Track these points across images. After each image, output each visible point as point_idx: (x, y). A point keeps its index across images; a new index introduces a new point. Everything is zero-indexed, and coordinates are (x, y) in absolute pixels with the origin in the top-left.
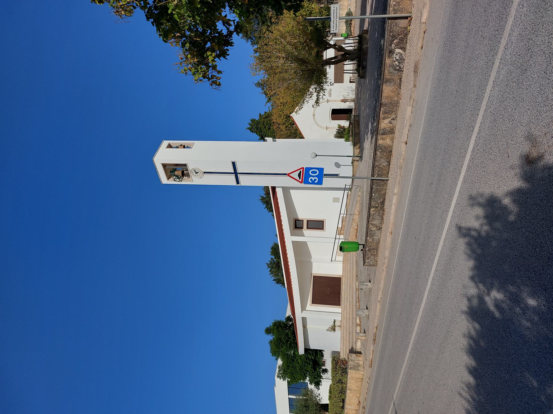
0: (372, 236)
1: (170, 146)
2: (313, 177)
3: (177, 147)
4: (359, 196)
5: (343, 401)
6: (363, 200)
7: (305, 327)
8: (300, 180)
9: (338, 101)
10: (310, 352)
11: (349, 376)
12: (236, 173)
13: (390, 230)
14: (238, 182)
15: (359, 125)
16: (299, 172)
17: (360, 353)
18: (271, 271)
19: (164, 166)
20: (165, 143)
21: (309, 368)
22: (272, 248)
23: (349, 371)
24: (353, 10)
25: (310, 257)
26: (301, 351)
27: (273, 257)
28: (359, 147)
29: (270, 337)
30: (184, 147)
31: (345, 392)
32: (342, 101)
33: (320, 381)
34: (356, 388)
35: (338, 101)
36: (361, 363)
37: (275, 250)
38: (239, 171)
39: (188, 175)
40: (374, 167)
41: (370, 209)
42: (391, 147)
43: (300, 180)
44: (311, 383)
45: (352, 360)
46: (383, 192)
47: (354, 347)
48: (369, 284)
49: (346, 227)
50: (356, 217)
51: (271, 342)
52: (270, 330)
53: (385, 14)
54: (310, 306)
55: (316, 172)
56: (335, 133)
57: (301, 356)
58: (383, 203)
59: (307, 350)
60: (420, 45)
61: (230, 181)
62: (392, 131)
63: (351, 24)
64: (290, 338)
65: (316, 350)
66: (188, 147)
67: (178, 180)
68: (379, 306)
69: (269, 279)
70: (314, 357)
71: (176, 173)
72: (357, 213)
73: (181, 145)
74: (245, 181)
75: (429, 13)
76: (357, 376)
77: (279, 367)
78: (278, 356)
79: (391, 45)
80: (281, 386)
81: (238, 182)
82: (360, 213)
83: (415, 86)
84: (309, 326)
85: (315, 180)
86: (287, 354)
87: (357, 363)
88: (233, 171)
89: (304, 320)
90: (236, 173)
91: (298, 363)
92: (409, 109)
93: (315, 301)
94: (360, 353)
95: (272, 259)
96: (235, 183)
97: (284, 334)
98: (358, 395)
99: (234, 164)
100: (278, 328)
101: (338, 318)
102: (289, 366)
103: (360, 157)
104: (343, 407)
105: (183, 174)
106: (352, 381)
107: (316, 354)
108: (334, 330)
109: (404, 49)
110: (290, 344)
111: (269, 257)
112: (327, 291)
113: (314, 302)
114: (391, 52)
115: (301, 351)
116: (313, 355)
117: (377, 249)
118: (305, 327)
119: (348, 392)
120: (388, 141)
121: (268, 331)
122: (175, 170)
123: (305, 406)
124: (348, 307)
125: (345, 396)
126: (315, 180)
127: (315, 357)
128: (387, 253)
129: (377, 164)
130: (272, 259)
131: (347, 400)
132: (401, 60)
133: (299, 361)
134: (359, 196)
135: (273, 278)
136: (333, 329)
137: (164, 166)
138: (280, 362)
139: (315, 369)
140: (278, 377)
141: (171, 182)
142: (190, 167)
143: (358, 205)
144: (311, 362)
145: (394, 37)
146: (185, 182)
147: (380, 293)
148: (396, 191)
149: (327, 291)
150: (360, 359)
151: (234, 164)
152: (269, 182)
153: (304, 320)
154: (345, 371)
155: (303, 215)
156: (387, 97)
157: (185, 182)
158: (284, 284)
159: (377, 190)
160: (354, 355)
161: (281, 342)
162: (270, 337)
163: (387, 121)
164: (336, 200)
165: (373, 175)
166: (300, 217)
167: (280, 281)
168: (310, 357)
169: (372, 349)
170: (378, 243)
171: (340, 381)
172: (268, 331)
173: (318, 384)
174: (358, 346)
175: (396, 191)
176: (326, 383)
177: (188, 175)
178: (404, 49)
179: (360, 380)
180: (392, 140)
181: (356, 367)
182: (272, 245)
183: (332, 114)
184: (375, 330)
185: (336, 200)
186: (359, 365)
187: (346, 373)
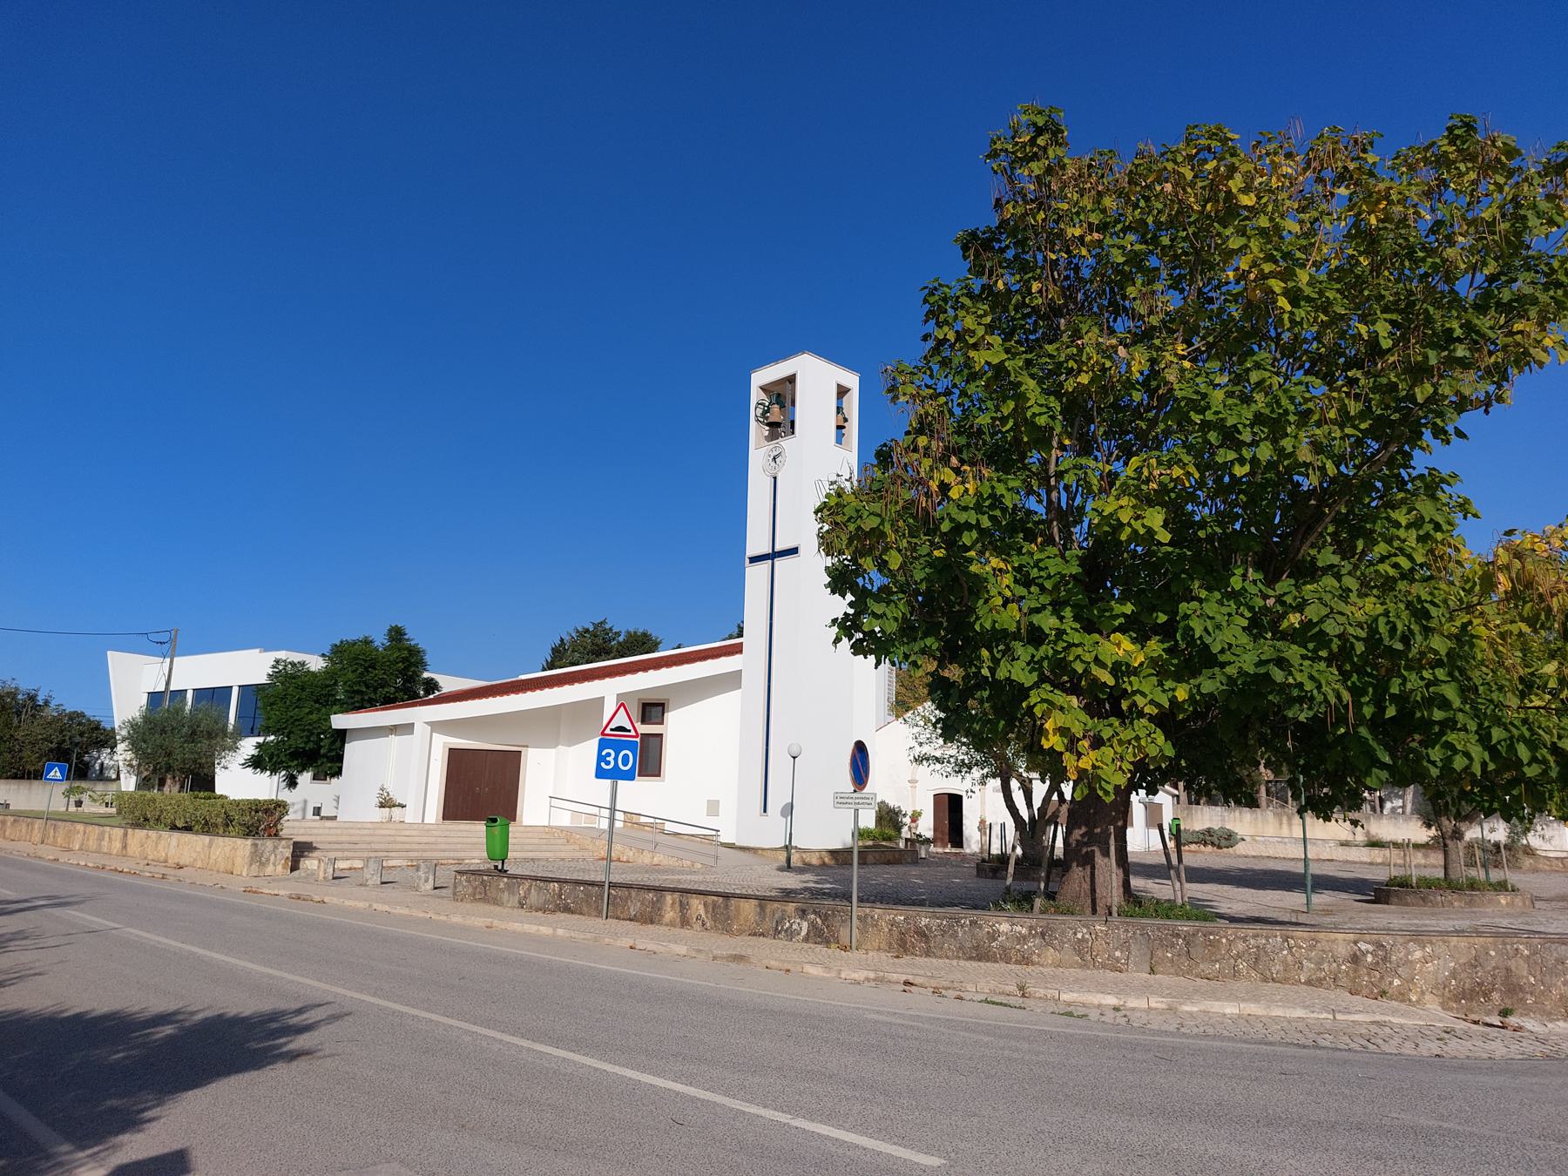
0: (509, 887)
1: (842, 392)
2: (616, 759)
3: (839, 409)
4: (693, 863)
5: (188, 829)
6: (679, 873)
7: (394, 729)
8: (608, 731)
9: (983, 810)
10: (338, 744)
11: (239, 841)
12: (773, 556)
13: (496, 923)
14: (754, 560)
15: (889, 863)
16: (629, 727)
17: (294, 868)
18: (587, 631)
19: (791, 379)
20: (852, 380)
21: (297, 742)
22: (645, 634)
23: (249, 842)
24: (1240, 848)
25: (571, 742)
26: (339, 721)
27: (621, 639)
28: (824, 864)
29: (380, 640)
30: (840, 427)
31: (208, 833)
32: (982, 822)
33: (263, 769)
34: (213, 857)
35: (983, 810)
36: (269, 870)
37: (642, 642)
38: (779, 562)
39: (773, 436)
40: (629, 887)
41: (558, 881)
42: (660, 923)
43: (608, 731)
44: (259, 746)
45: (276, 848)
46: (585, 909)
47: (316, 854)
48: (430, 885)
49: (639, 834)
50: (646, 859)
51: (367, 642)
52: (400, 640)
53: (861, 900)
54: (442, 743)
55: (625, 764)
56: (891, 805)
57: (328, 720)
58: (567, 909)
59: (342, 736)
60: (772, 963)
61: (757, 543)
62: (685, 922)
63: (1205, 844)
64: (375, 691)
65: (340, 758)
66: (839, 441)
67: (760, 411)
68: (361, 905)
69: (566, 628)
70: (320, 755)
71: (776, 408)
72: (656, 861)
73: (846, 420)
74: (756, 576)
75: (816, 978)
76: (238, 861)
77: (303, 664)
78: (331, 659)
79: (815, 912)
80: (248, 667)
81: (754, 560)
82: (655, 868)
83: (715, 958)
84: (394, 739)
85: (608, 763)
86: (336, 684)
87: (268, 860)
88: (778, 548)
89: (408, 728)
90: (773, 556)
91: (311, 713)
92: (682, 949)
93: (456, 758)
94: (294, 868)
95: (618, 634)
96: (752, 551)
97: (388, 676)
98: (199, 864)
99: (794, 551)
100: (404, 660)
101: (410, 815)
102: (303, 689)
103: (789, 866)
104: (174, 828)
105: (774, 425)
106: (227, 849)
107: (331, 760)
108: (382, 806)
109: (806, 939)
110: (359, 692)
111: (622, 624)
112: (482, 786)
113: (454, 754)
114: (803, 913)
115: (339, 721)
116: (330, 750)
117: (485, 900)
118: (394, 729)
119: (207, 839)
120: (670, 914)
121: (397, 634)
122: (782, 406)
123: (194, 733)
124: (425, 840)
125: (197, 833)
126: (608, 763)
127: (324, 756)
128: (456, 919)
129: (633, 893)
130: (618, 634)
131: (188, 837)
132: (791, 934)
133: (314, 717)
134: (693, 863)
135: (567, 638)
136: (387, 803)
137: (791, 379)
138: (316, 663)
139: (295, 755)
140: (277, 661)
141: (756, 396)
142: (786, 443)
143: (672, 862)
144: (311, 745)
145: (825, 918)
146: (756, 431)
147: (386, 908)
148: (560, 932)
149: (482, 786)
150: (279, 868)
151: (794, 551)
152: (754, 637)
153: (408, 728)
154: (250, 831)
155: (677, 727)
156: (738, 909)
157: (756, 431)
158: (551, 666)
159: (588, 895)
160: (288, 853)
161: (366, 669)
162: (380, 640)
163: (701, 907)
164: (713, 808)
165: (612, 885)
166: (670, 717)
167: (559, 656)
168: (325, 743)
169: (282, 892)
170: (496, 902)
171: (228, 821)
172: (397, 634)
173: (256, 763)
174: (309, 864)
175: (560, 932)
176: (263, 786)
177: (773, 436)
178: (806, 939)
179: (229, 867)
180: (672, 924)
181: (257, 858)
182: (654, 633)
183: (950, 795)
184: (317, 898)
185: (713, 808)
186: (263, 865)
187: (247, 835)
